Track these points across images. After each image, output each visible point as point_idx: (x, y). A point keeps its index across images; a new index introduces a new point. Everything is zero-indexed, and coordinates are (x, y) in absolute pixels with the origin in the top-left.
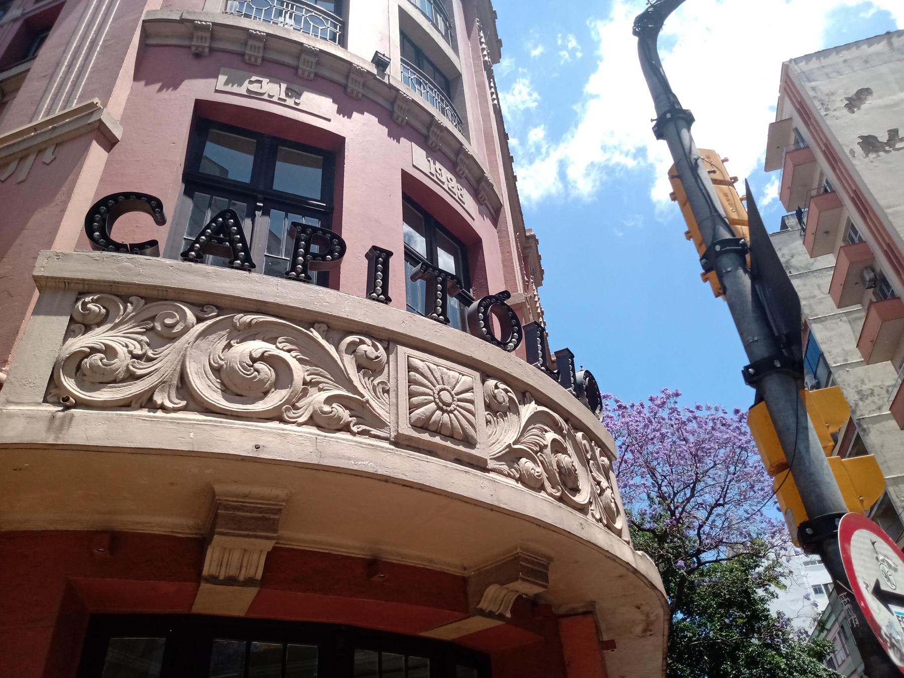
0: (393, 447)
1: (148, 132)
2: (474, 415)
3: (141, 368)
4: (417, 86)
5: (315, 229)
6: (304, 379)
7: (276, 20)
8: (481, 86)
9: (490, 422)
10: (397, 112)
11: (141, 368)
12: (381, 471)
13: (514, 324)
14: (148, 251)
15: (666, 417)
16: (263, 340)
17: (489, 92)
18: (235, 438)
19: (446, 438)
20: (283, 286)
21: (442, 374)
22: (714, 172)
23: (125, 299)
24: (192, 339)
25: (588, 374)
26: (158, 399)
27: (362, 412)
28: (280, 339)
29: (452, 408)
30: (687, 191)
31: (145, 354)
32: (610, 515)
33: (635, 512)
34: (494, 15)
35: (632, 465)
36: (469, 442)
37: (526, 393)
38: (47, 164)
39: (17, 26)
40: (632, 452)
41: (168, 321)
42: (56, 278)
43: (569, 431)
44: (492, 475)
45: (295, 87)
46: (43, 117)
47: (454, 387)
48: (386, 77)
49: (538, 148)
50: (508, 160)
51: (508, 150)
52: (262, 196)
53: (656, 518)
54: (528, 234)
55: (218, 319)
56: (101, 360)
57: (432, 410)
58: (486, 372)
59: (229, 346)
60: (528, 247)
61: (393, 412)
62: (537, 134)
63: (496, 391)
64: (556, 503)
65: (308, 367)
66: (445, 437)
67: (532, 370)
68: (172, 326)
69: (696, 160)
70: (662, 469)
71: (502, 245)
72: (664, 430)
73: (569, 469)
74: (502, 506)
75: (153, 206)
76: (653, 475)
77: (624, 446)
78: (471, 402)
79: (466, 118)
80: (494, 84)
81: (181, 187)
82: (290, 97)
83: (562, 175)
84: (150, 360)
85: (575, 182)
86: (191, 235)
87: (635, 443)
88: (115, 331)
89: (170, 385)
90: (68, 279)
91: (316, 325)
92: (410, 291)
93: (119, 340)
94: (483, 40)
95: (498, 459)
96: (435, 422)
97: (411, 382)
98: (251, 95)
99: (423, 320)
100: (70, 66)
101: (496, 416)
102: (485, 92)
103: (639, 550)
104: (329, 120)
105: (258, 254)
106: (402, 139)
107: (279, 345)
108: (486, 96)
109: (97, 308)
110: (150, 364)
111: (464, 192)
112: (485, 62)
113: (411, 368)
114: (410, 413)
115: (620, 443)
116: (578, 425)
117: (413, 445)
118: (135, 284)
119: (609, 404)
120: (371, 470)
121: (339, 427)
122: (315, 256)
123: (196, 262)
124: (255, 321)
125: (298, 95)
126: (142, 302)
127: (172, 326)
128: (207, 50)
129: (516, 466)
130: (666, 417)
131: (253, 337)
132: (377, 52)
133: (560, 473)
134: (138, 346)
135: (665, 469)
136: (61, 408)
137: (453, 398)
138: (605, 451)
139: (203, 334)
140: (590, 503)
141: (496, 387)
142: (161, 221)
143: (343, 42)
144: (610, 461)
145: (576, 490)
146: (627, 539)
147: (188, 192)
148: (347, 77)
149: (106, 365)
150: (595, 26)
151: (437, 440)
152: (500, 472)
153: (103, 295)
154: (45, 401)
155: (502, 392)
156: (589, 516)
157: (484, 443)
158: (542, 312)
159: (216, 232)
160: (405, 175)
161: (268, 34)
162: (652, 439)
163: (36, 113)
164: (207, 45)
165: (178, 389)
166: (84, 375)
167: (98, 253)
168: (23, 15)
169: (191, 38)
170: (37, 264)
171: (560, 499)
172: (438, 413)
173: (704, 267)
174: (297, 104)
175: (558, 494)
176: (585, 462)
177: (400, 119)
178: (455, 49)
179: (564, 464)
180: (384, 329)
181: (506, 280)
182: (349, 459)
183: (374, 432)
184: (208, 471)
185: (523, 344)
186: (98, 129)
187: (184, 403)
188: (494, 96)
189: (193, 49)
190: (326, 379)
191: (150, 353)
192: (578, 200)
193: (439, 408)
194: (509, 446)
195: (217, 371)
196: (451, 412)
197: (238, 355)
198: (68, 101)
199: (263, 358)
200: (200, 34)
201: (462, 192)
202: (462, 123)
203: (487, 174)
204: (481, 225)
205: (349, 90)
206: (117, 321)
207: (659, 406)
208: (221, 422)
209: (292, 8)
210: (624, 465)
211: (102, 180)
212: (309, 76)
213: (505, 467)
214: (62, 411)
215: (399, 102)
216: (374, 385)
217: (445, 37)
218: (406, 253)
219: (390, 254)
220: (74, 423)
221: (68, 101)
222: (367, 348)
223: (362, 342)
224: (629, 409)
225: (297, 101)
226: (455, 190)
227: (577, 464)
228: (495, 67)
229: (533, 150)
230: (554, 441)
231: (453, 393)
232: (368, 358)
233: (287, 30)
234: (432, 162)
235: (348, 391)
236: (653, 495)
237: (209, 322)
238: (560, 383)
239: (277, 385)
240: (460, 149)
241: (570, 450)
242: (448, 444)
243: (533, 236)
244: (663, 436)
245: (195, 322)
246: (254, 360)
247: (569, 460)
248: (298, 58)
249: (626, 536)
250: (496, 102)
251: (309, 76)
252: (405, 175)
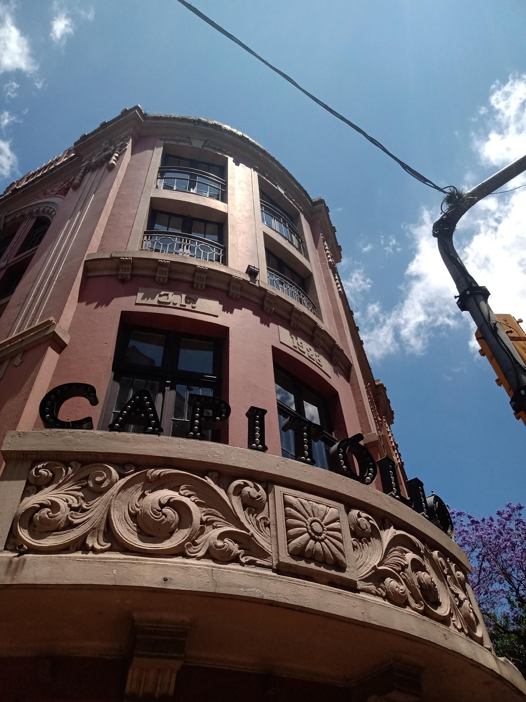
0: (275, 574)
1: (87, 337)
2: (342, 542)
4: (280, 286)
5: (206, 398)
6: (201, 519)
7: (177, 251)
8: (328, 280)
9: (356, 547)
10: (266, 305)
12: (266, 597)
13: (371, 460)
14: (85, 425)
15: (513, 527)
16: (169, 489)
17: (334, 283)
18: (146, 573)
19: (319, 564)
20: (184, 444)
21: (312, 507)
22: (511, 332)
23: (67, 465)
24: (116, 492)
25: (437, 499)
26: (90, 542)
27: (248, 544)
28: (182, 487)
29: (322, 537)
30: (491, 347)
31: (80, 506)
32: (470, 625)
33: (499, 616)
34: (334, 230)
35: (490, 572)
36: (340, 566)
37: (385, 520)
38: (17, 366)
39: (4, 272)
40: (489, 561)
41: (98, 479)
42: (17, 451)
43: (425, 550)
44: (362, 595)
45: (192, 296)
46: (16, 333)
47: (324, 518)
48: (257, 282)
49: (377, 319)
50: (354, 330)
51: (354, 322)
52: (170, 374)
53: (518, 620)
54: (377, 384)
55: (135, 474)
56: (48, 513)
57: (306, 540)
58: (350, 503)
59: (143, 496)
60: (378, 395)
61: (274, 543)
62: (374, 309)
63: (359, 519)
65: (204, 509)
66: (319, 564)
67: (389, 499)
68: (101, 483)
69: (495, 324)
70: (517, 575)
71: (355, 395)
72: (514, 540)
73: (429, 585)
74: (372, 622)
75: (88, 391)
76: (510, 582)
77: (481, 557)
78: (339, 530)
79: (318, 304)
80: (339, 277)
81: (111, 374)
82: (189, 303)
83: (397, 337)
84: (84, 511)
85: (408, 341)
86: (118, 410)
87: (490, 552)
88: (59, 489)
89: (98, 531)
90: (26, 451)
91: (210, 474)
92: (284, 439)
93: (60, 496)
94: (327, 248)
95: (366, 580)
96: (309, 550)
97: (288, 516)
98: (161, 304)
99: (293, 463)
100: (35, 296)
101: (361, 542)
102: (332, 284)
103: (502, 656)
104: (217, 316)
105: (167, 422)
106: (271, 324)
107: (181, 492)
108: (332, 287)
109: (46, 473)
110: (84, 514)
111: (321, 358)
112: (330, 263)
113: (287, 504)
114: (288, 543)
115: (477, 554)
116: (433, 545)
117: (292, 571)
118: (75, 452)
119: (461, 523)
120: (258, 596)
121: (230, 559)
122: (208, 418)
123: (120, 431)
124: (163, 474)
125: (195, 301)
126: (79, 465)
127: (101, 483)
128: (129, 277)
129: (382, 585)
130: (513, 527)
131: (161, 487)
132: (249, 265)
133: (421, 589)
134: (75, 500)
135: (519, 574)
136: (17, 554)
137: (323, 528)
138: (460, 566)
139: (124, 488)
140: (451, 615)
141: (359, 516)
142: (94, 402)
143: (225, 261)
144: (465, 573)
145: (437, 604)
146: (489, 647)
147: (116, 378)
148: (229, 285)
149: (51, 517)
150: (408, 229)
151: (312, 566)
152: (368, 592)
153: (51, 462)
154: (6, 549)
155: (365, 520)
156: (452, 627)
157: (352, 567)
158: (396, 445)
159: (134, 406)
160: (275, 350)
161: (171, 262)
162: (504, 548)
163: (11, 331)
164: (129, 273)
165: (105, 534)
166: (35, 526)
167: (48, 430)
168: (7, 265)
169: (118, 270)
170: (4, 442)
171: (424, 613)
172: (312, 542)
173: (514, 408)
174: (194, 308)
175: (422, 608)
176: (442, 577)
177: (269, 310)
178: (307, 256)
179: (424, 581)
180: (263, 472)
181: (361, 423)
182: (240, 586)
183: (259, 561)
184: (128, 602)
185: (378, 476)
186: (53, 338)
187: (109, 545)
188: (339, 286)
189: (120, 277)
190: (219, 520)
191: (84, 506)
192: (412, 355)
193: (312, 538)
194: (374, 568)
195: (134, 516)
196: (323, 540)
197: (150, 503)
198: (33, 320)
199: (171, 504)
200: (124, 266)
201: (319, 358)
202: (315, 307)
203: (338, 342)
204: (337, 382)
205: (230, 294)
206: (60, 481)
207: (507, 519)
208: (137, 560)
209: (188, 242)
210: (483, 573)
211: (54, 375)
212: (201, 287)
213: (372, 587)
214: (18, 556)
215: (267, 298)
216: (257, 521)
217: (299, 249)
218: (278, 408)
219: (265, 412)
220: (26, 566)
221: (33, 320)
222: (250, 490)
223: (246, 485)
224: (481, 524)
225: (194, 305)
226: (314, 357)
227: (435, 579)
228: (338, 266)
229: (373, 321)
230: (414, 561)
231: (322, 523)
232: (251, 497)
233: (185, 258)
234: (294, 338)
235: (237, 527)
236: (513, 598)
237: (128, 478)
238: (414, 509)
239: (180, 525)
240: (315, 327)
241: (429, 567)
242: (322, 569)
243: (382, 385)
244: (514, 545)
245: (118, 478)
246: (162, 506)
247: (428, 576)
248: (194, 276)
249: (488, 643)
250: (340, 290)
251: (201, 287)
252: (275, 350)
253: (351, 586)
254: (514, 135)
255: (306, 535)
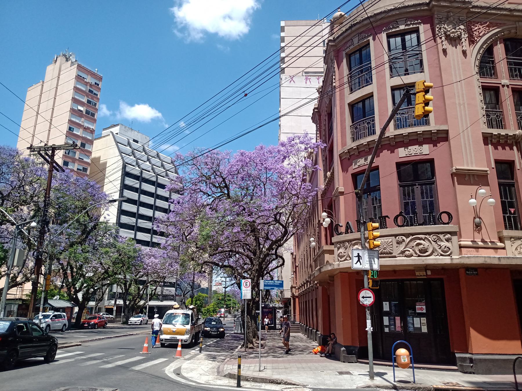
66: (386, 254)
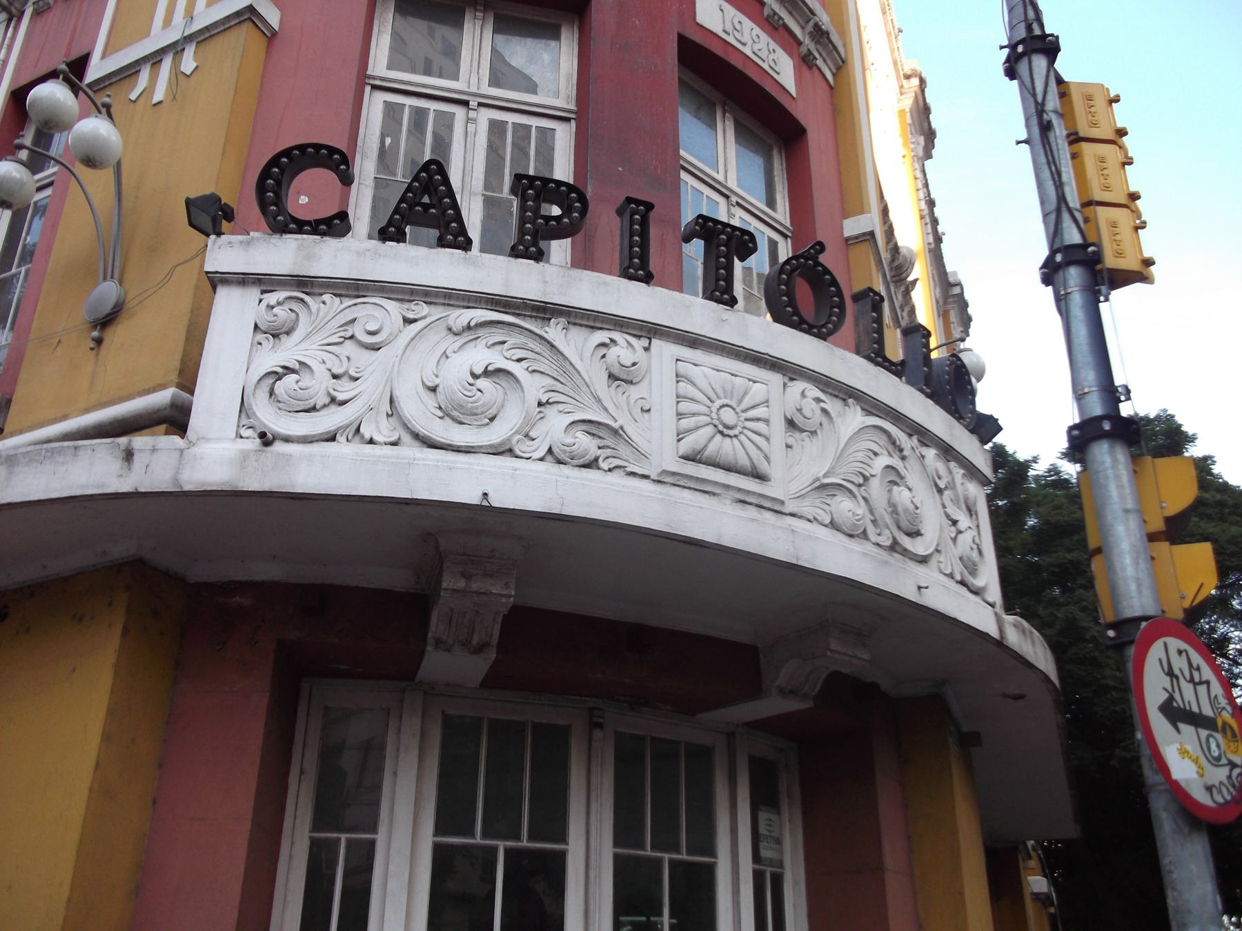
2: (767, 439)
3: (344, 390)
11: (344, 390)
29: (736, 432)
64: (884, 555)
78: (767, 421)
89: (378, 413)
97: (679, 398)
141: (803, 394)
196: (736, 436)
226: (764, 54)
231: (738, 410)
253: (775, 508)
254: (1035, 460)
255: (709, 430)
